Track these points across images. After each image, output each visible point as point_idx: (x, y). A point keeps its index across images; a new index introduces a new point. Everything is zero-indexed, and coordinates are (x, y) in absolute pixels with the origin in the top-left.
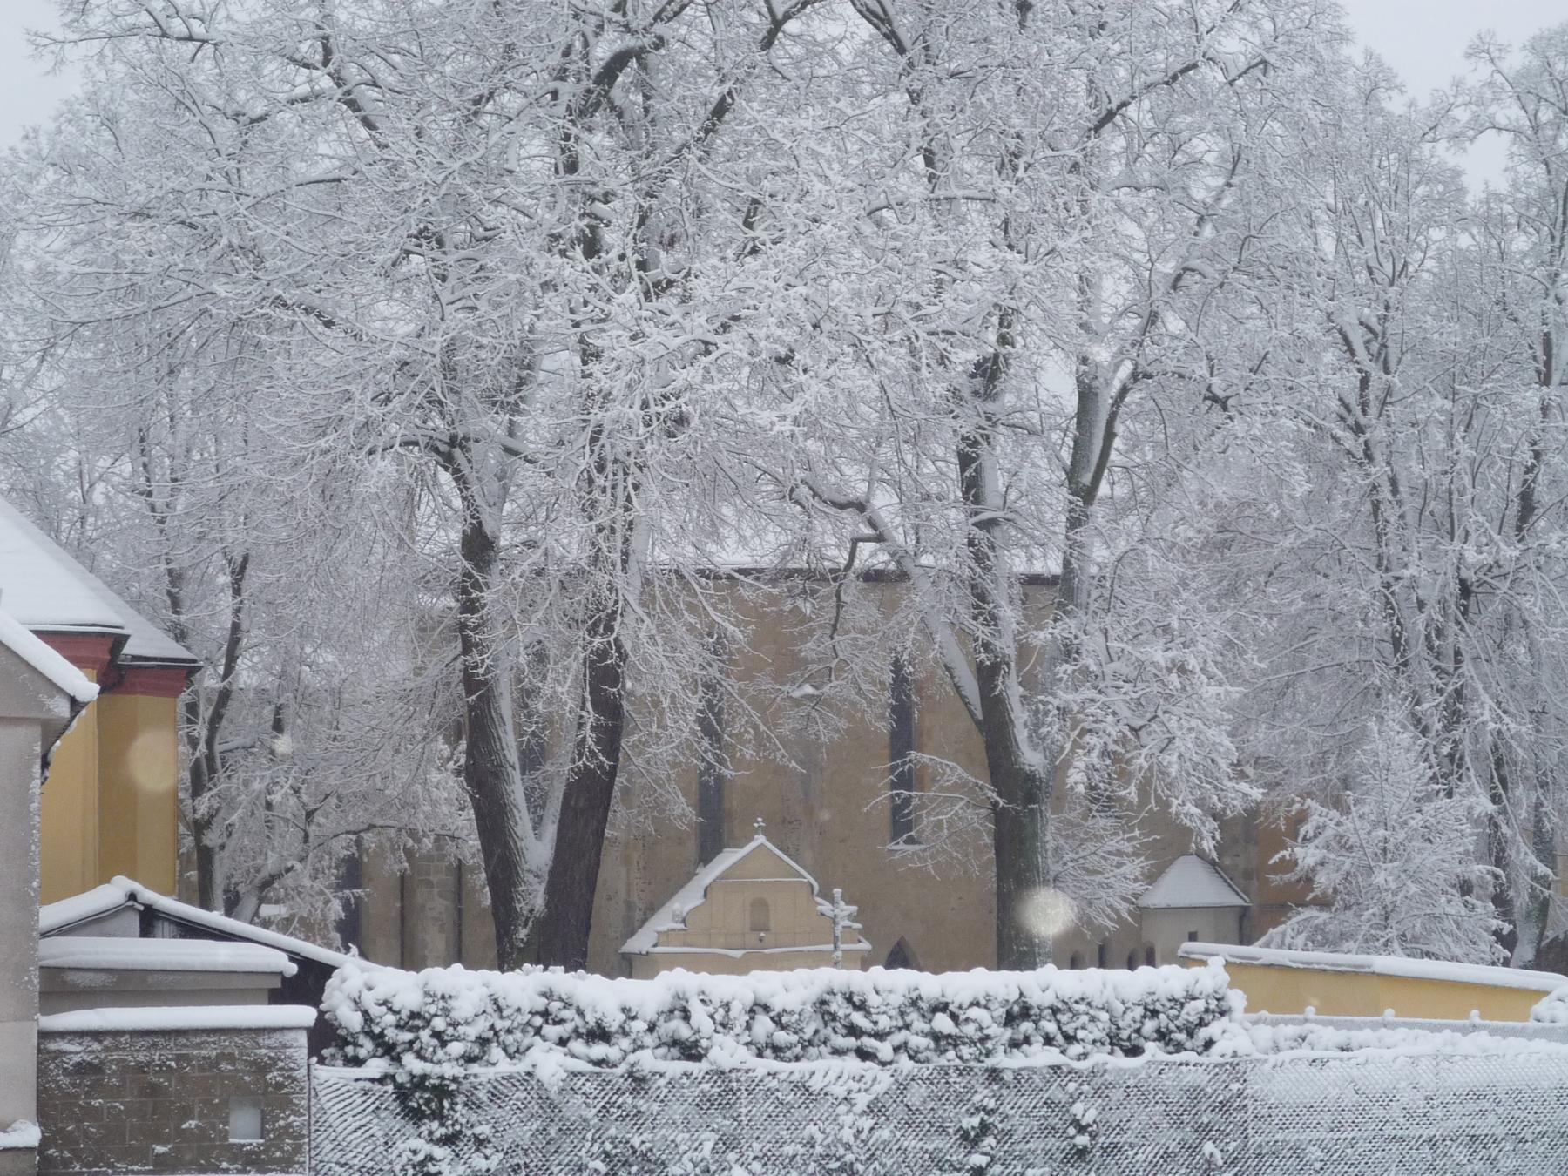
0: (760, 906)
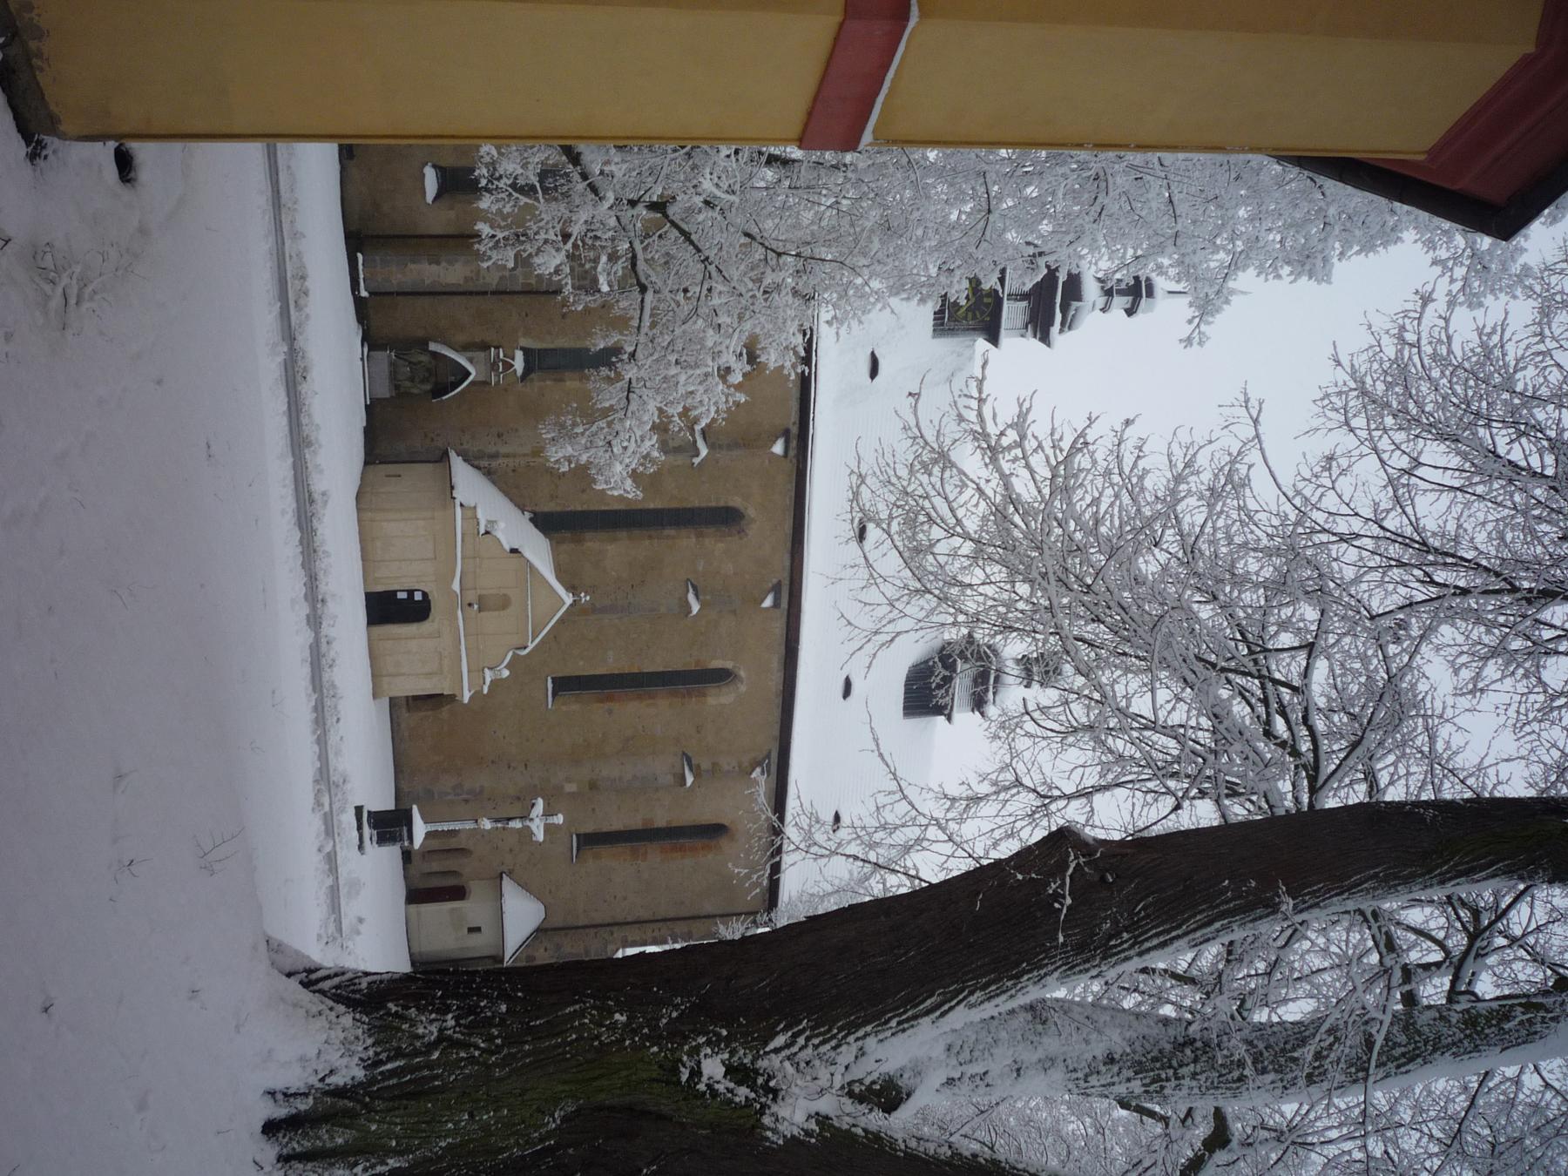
0: (504, 603)
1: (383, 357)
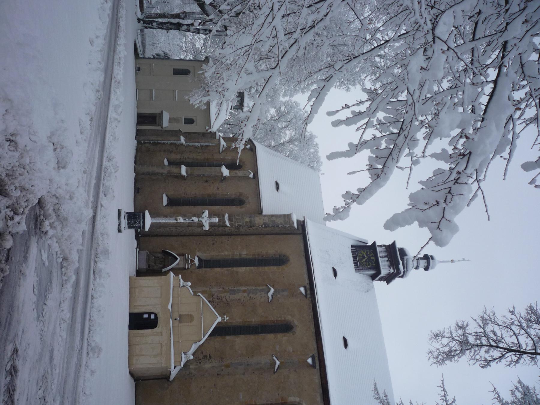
0: (191, 318)
1: (144, 253)
